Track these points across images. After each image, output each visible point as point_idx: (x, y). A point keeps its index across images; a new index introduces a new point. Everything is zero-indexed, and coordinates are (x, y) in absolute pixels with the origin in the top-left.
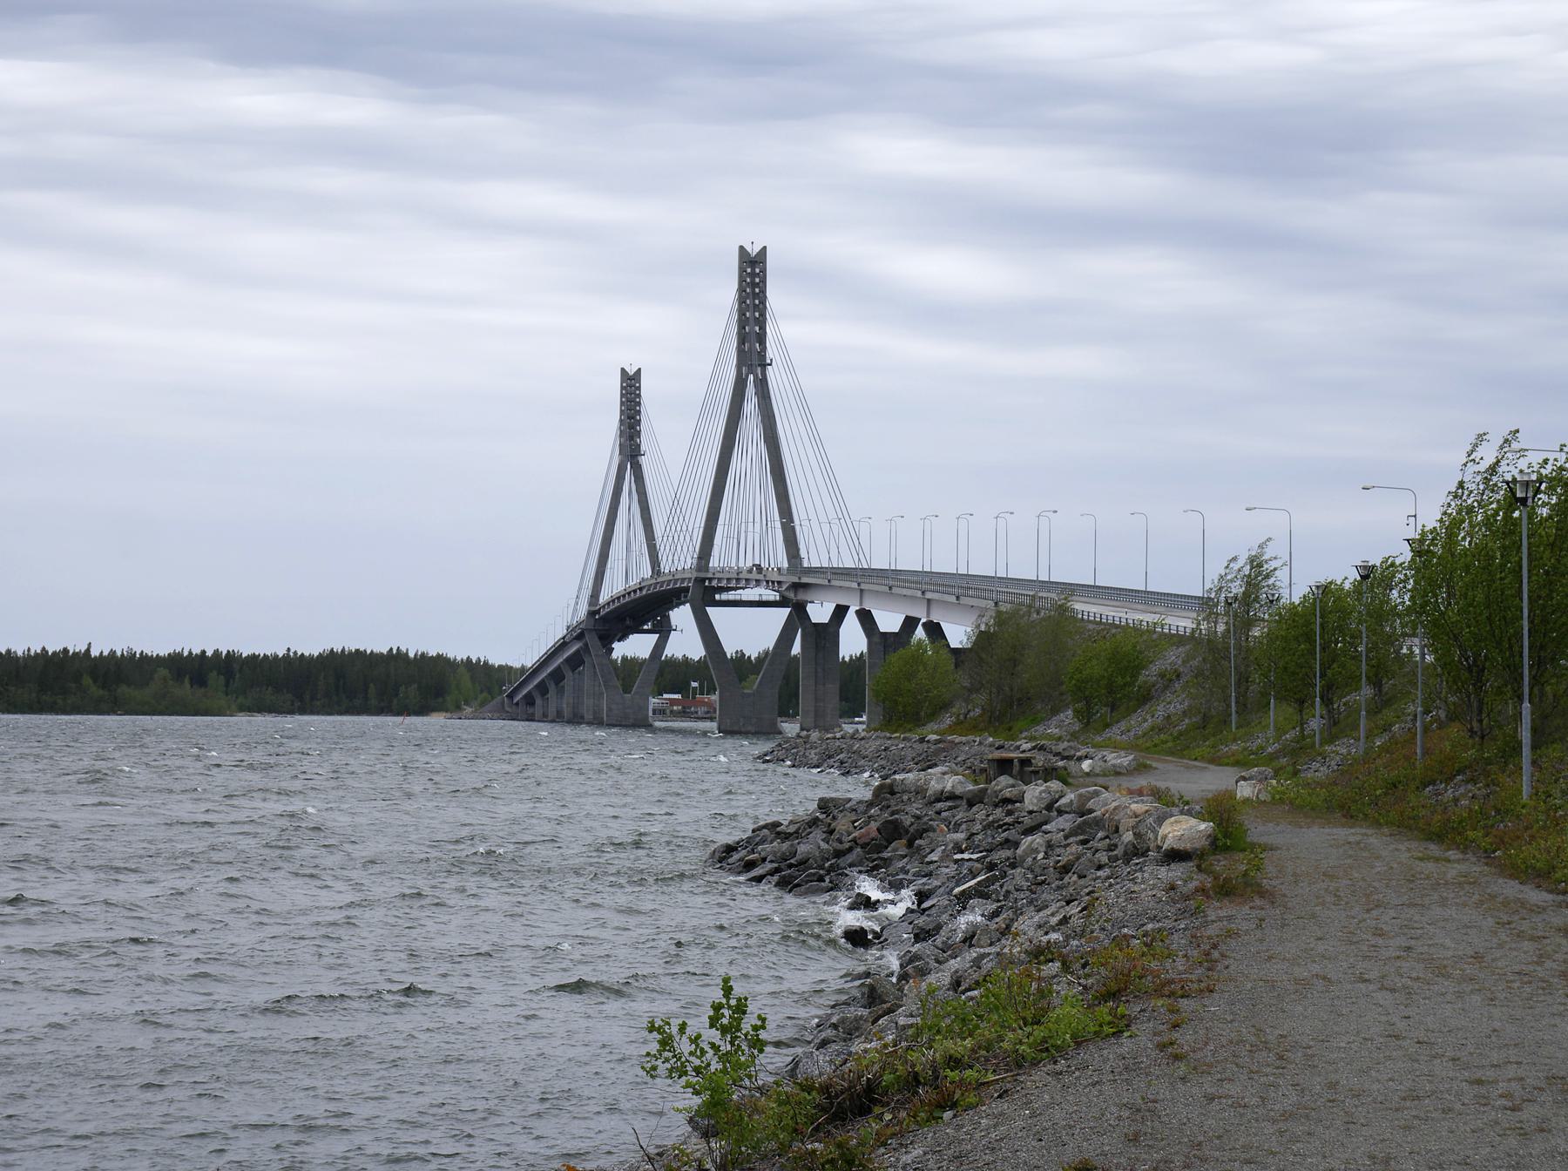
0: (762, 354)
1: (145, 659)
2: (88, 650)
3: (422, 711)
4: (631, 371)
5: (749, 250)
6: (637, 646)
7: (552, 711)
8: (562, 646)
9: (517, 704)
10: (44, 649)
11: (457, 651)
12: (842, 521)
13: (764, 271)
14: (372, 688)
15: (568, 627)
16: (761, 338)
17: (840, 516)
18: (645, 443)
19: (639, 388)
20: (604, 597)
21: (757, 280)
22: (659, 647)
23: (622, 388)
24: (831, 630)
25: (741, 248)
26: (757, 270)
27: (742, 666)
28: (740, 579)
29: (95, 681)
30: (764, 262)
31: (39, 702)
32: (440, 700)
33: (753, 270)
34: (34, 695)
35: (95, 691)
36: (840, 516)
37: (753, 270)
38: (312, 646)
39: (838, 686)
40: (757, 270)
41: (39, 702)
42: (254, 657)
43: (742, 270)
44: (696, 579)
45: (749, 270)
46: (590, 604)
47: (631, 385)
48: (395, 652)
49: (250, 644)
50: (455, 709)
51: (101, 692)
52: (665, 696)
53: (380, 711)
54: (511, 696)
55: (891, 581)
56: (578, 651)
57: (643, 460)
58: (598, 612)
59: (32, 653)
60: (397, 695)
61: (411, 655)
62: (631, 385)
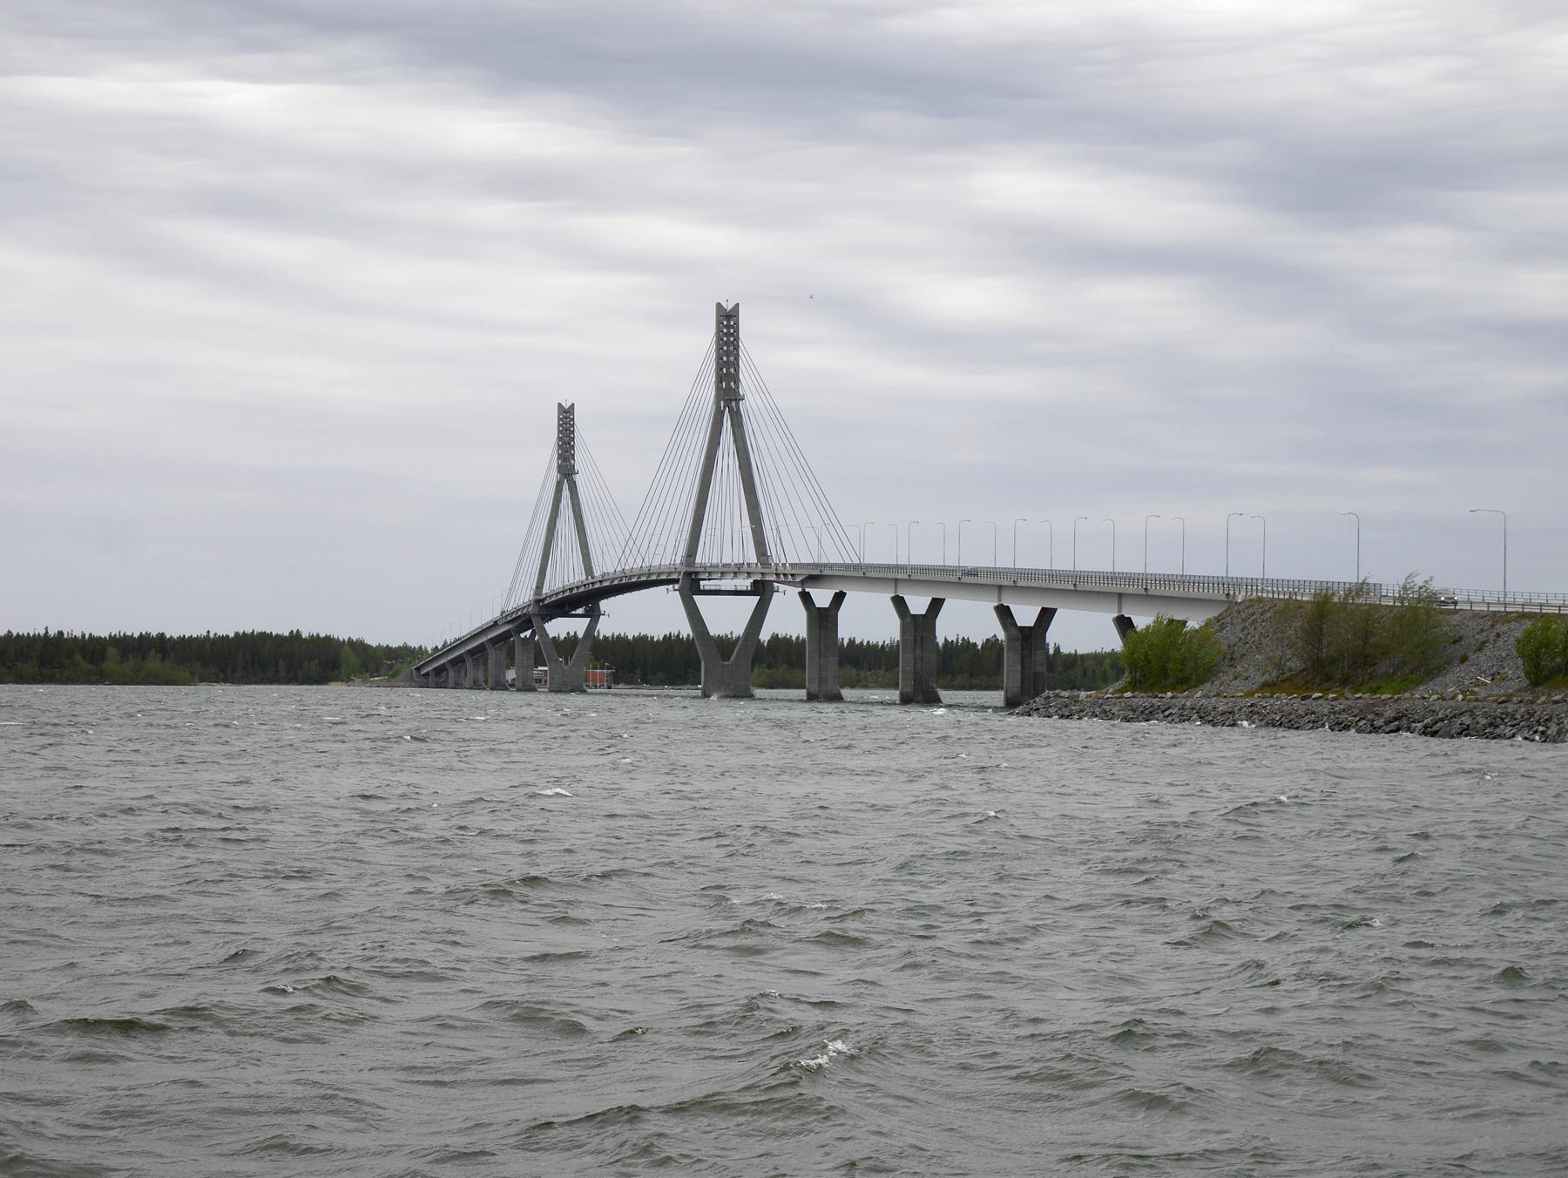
0: (736, 391)
1: (93, 640)
2: (47, 632)
3: (322, 680)
4: (567, 405)
5: (725, 306)
6: (559, 628)
7: (469, 680)
8: (495, 624)
9: (427, 674)
10: (9, 632)
11: (342, 634)
12: (830, 527)
13: (737, 323)
14: (281, 663)
15: (503, 612)
16: (736, 379)
17: (827, 521)
18: (579, 462)
19: (573, 419)
20: (545, 590)
21: (732, 331)
22: (591, 628)
23: (559, 419)
24: (832, 613)
25: (719, 305)
26: (732, 323)
27: (724, 646)
28: (724, 571)
29: (84, 658)
30: (737, 316)
31: (41, 675)
32: (337, 672)
33: (728, 322)
34: (37, 669)
35: (85, 665)
36: (827, 521)
37: (728, 322)
38: (226, 627)
39: (837, 659)
40: (732, 323)
41: (41, 675)
42: (182, 639)
43: (719, 323)
44: (685, 573)
45: (725, 323)
46: (536, 594)
47: (566, 416)
48: (87, 637)
49: (173, 631)
50: (347, 679)
51: (90, 667)
52: (540, 668)
53: (288, 681)
54: (418, 669)
55: (893, 578)
56: (508, 631)
57: (577, 478)
58: (543, 600)
59: (212, 635)
60: (301, 668)
61: (630, 637)
62: (566, 416)
